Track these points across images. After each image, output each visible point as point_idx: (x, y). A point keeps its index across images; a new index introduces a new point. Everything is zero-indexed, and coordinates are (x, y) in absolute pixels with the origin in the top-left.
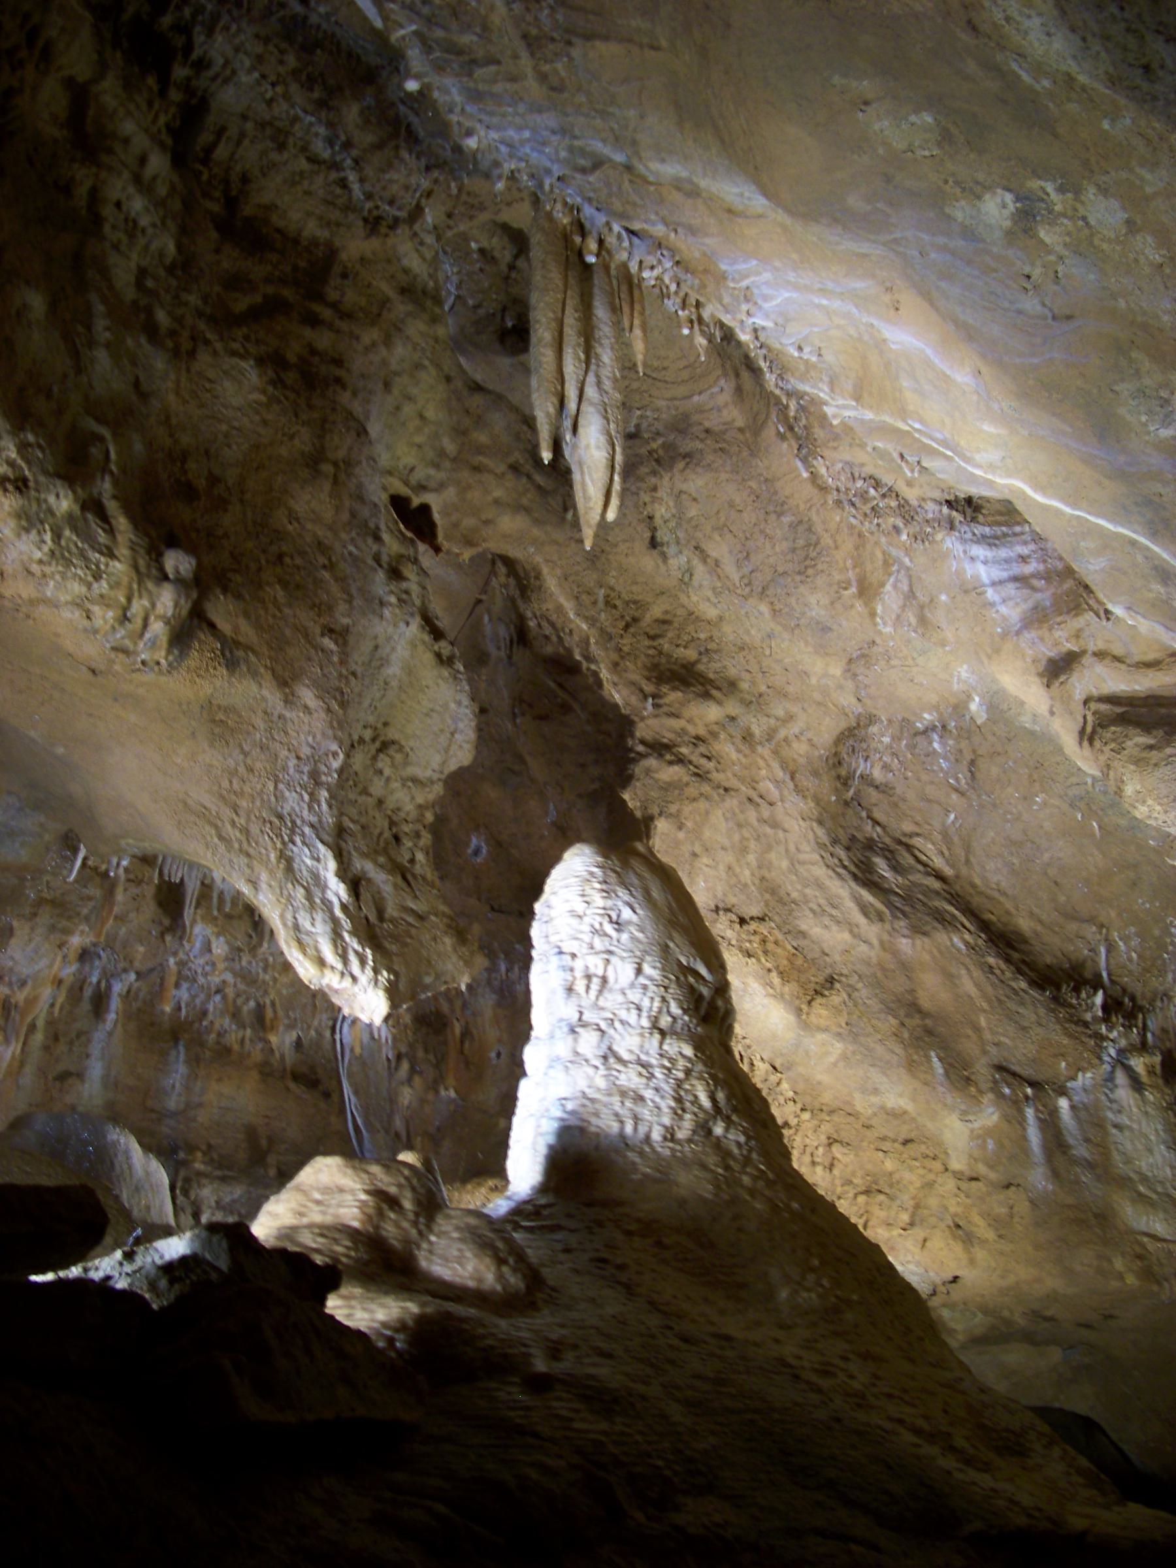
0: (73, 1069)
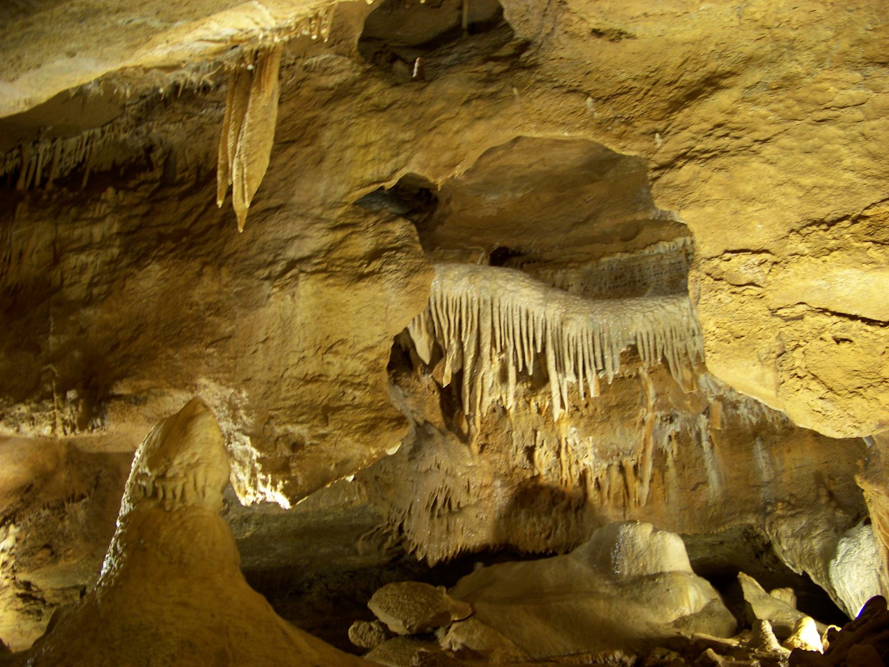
0: (701, 480)
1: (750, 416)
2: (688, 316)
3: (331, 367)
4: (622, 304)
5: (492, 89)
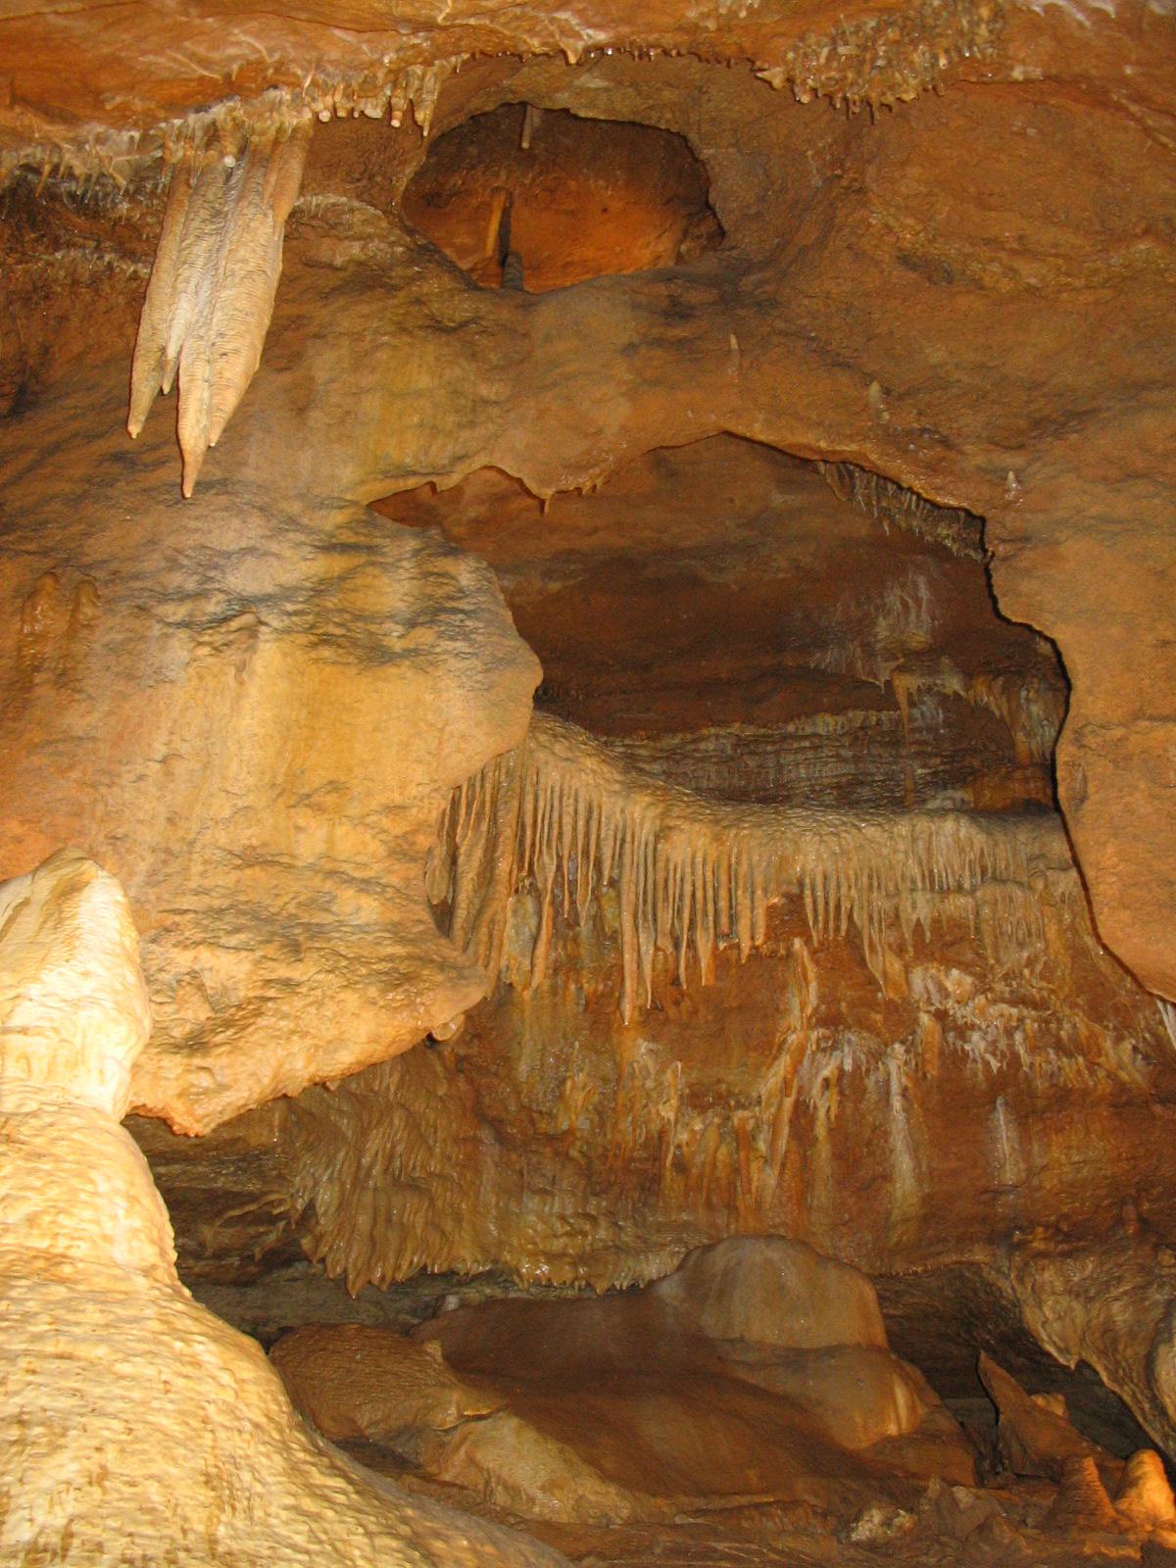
1: (988, 1057)
2: (906, 852)
3: (302, 837)
4: (777, 813)
5: (679, 332)
